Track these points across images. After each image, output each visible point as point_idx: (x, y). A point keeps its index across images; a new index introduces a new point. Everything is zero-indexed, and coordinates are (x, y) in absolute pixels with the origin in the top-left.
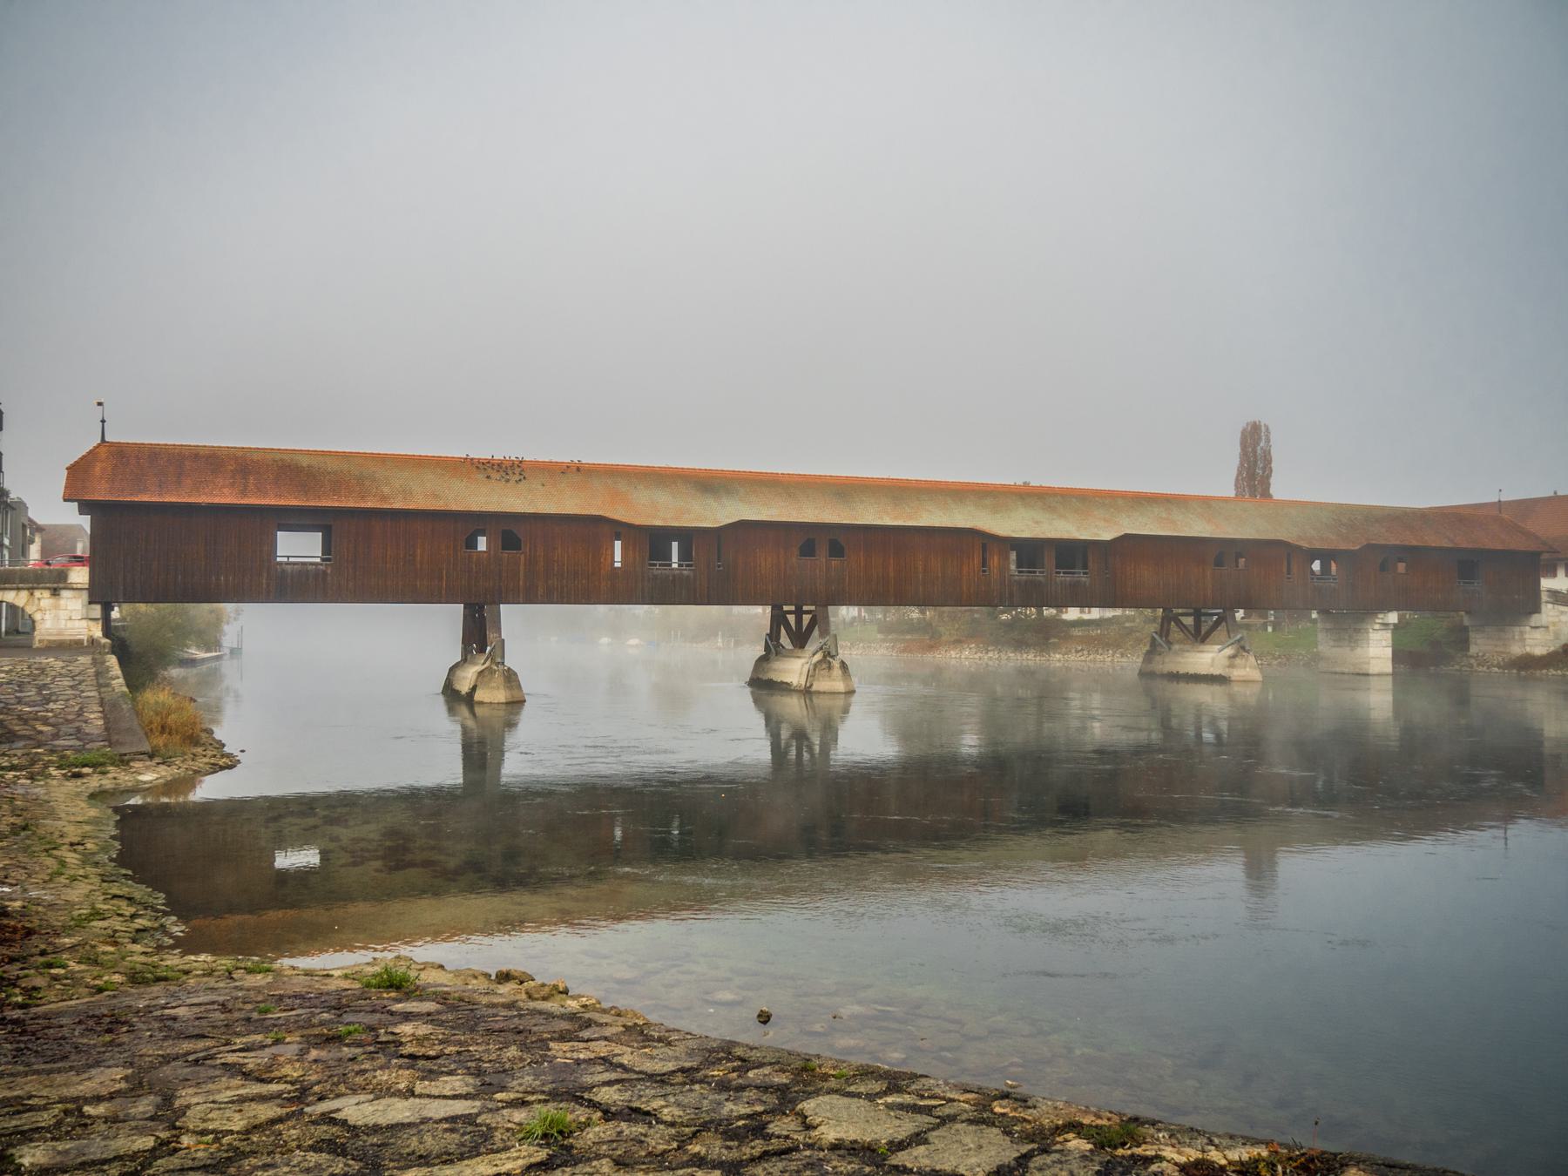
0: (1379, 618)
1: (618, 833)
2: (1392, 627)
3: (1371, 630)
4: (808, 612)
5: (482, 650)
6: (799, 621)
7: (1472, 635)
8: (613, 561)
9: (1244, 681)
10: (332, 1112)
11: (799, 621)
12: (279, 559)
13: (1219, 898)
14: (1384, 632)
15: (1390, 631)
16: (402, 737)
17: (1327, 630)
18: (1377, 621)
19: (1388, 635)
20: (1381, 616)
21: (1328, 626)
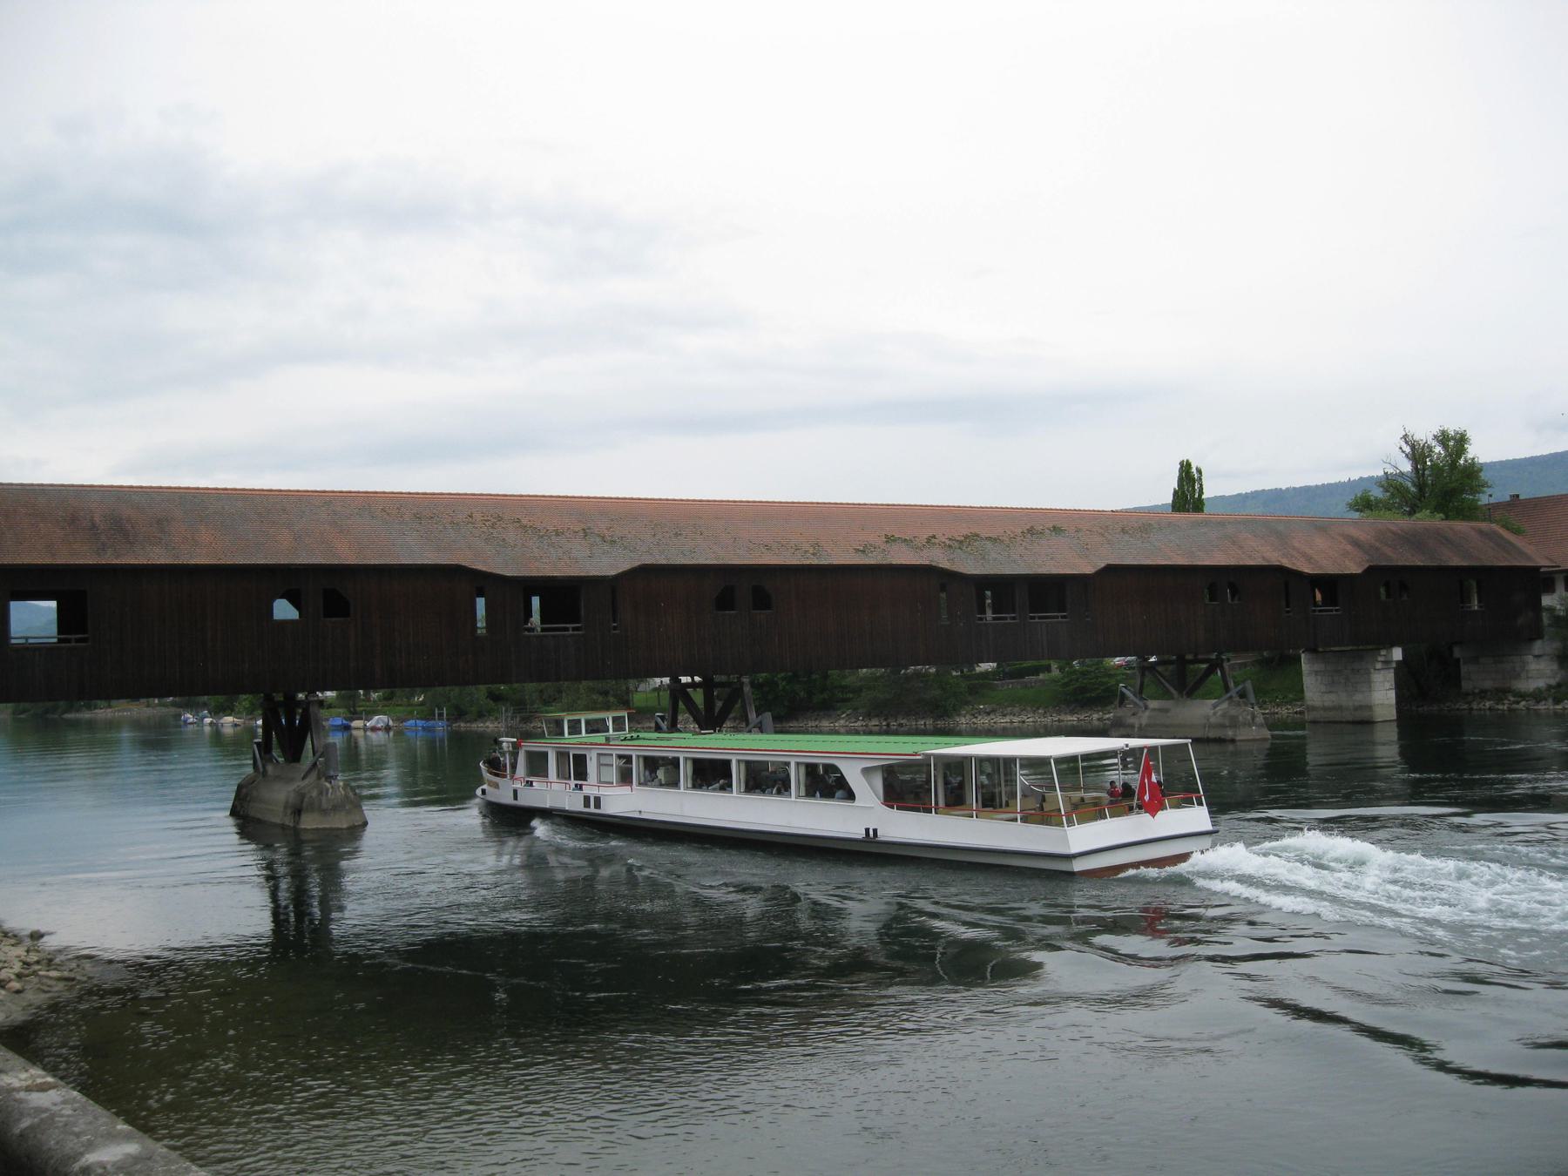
0: (1381, 656)
1: (309, 1020)
2: (1394, 665)
3: (1372, 671)
4: (722, 685)
5: (294, 755)
6: (291, 720)
7: (1464, 669)
8: (475, 627)
9: (1329, 722)
10: (1252, 914)
11: (291, 720)
12: (13, 641)
13: (1044, 1015)
14: (1386, 671)
15: (1392, 671)
16: (186, 885)
17: (1317, 673)
18: (1380, 659)
19: (1391, 675)
20: (1383, 652)
21: (1317, 667)
